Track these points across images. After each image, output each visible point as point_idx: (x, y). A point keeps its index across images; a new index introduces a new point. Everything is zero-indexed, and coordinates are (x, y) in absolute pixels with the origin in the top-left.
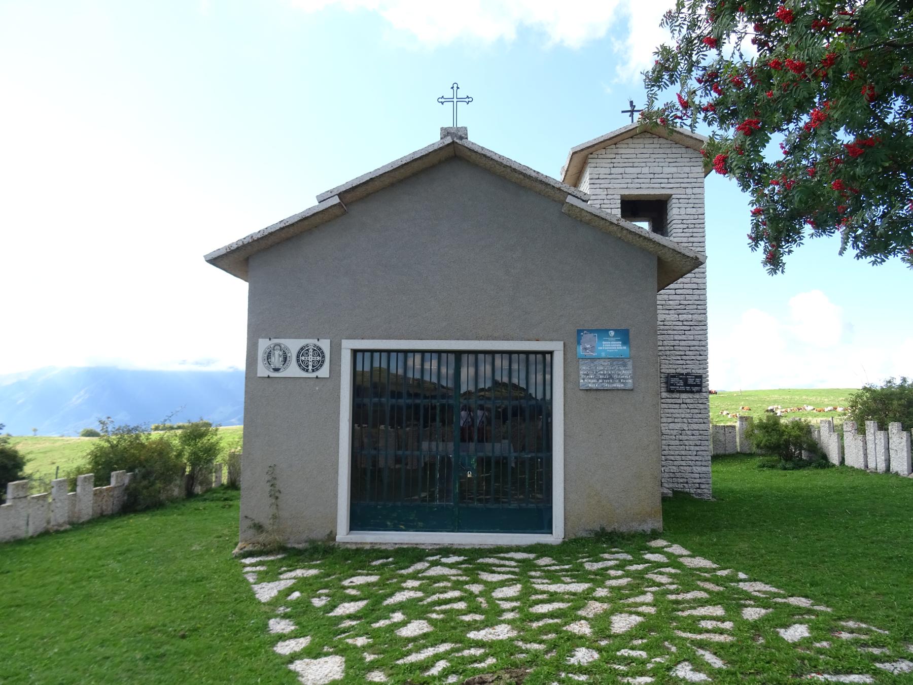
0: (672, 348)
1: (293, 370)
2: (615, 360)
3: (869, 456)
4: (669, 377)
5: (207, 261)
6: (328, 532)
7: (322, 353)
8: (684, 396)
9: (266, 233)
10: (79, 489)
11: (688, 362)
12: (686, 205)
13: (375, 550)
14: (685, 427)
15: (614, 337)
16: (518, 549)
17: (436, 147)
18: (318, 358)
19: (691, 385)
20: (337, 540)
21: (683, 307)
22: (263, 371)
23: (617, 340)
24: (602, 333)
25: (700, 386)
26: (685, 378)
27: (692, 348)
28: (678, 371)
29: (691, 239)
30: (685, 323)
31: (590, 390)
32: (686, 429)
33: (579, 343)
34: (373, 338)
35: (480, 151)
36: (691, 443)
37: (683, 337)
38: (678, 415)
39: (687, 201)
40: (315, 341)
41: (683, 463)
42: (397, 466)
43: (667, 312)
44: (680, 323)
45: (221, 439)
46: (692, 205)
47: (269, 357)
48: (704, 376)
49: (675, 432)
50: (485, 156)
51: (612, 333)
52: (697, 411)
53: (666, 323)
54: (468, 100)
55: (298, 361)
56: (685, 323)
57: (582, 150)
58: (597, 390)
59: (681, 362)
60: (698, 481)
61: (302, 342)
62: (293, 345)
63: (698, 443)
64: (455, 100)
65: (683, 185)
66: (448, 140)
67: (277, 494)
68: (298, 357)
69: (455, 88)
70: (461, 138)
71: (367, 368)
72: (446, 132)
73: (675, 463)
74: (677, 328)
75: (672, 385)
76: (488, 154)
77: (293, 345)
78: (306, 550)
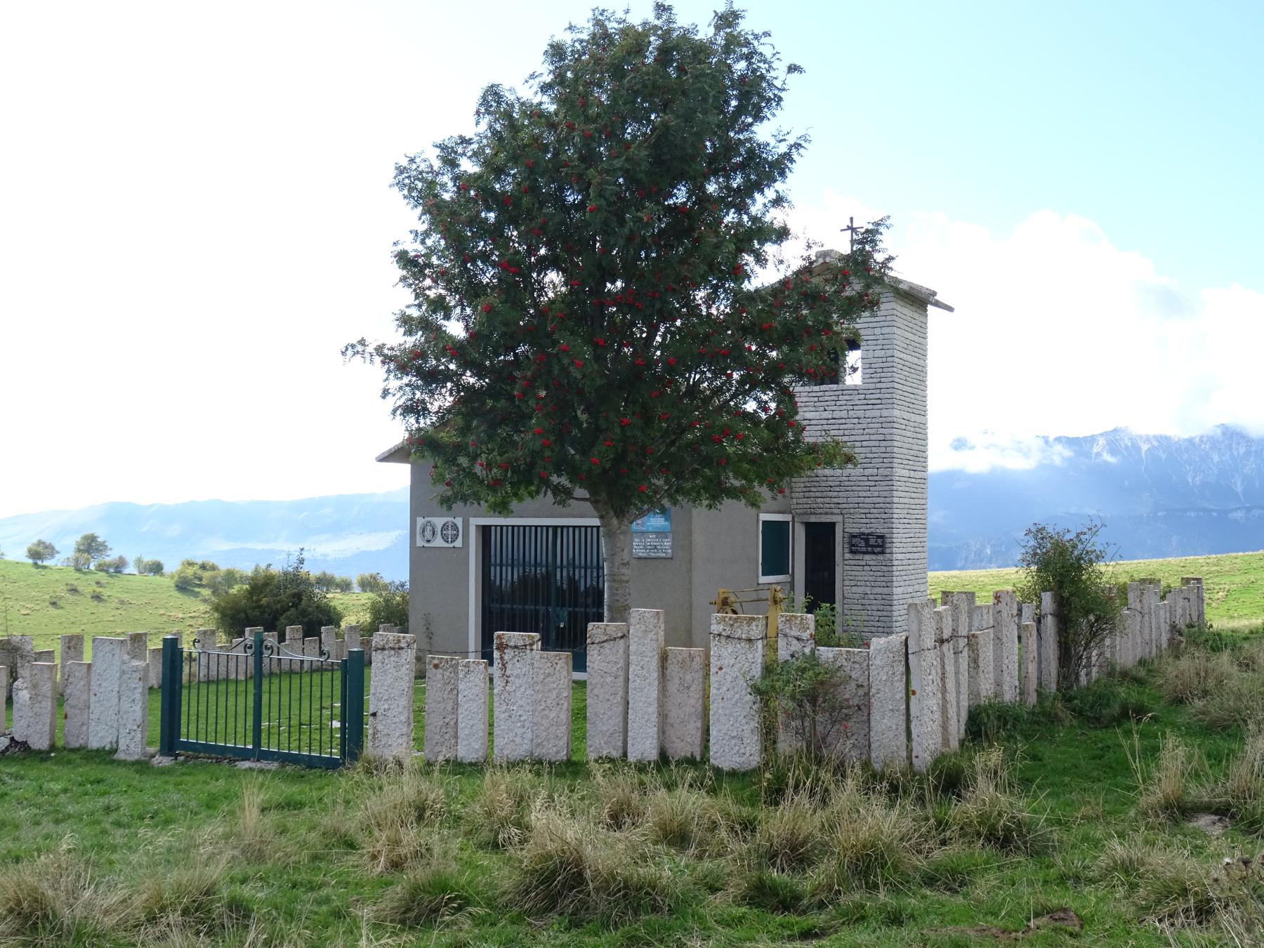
1: (439, 542)
2: (661, 534)
4: (853, 536)
8: (867, 557)
12: (875, 348)
14: (868, 590)
18: (455, 532)
19: (872, 546)
21: (868, 460)
22: (420, 542)
26: (865, 537)
27: (877, 506)
28: (862, 530)
29: (879, 385)
30: (870, 478)
31: (640, 558)
32: (869, 592)
36: (873, 607)
37: (868, 494)
38: (861, 578)
39: (875, 342)
40: (452, 519)
41: (866, 629)
44: (866, 479)
46: (881, 347)
47: (423, 531)
52: (880, 574)
53: (851, 478)
56: (870, 478)
58: (645, 558)
59: (865, 521)
63: (881, 608)
65: (871, 325)
68: (442, 531)
74: (862, 483)
75: (853, 545)
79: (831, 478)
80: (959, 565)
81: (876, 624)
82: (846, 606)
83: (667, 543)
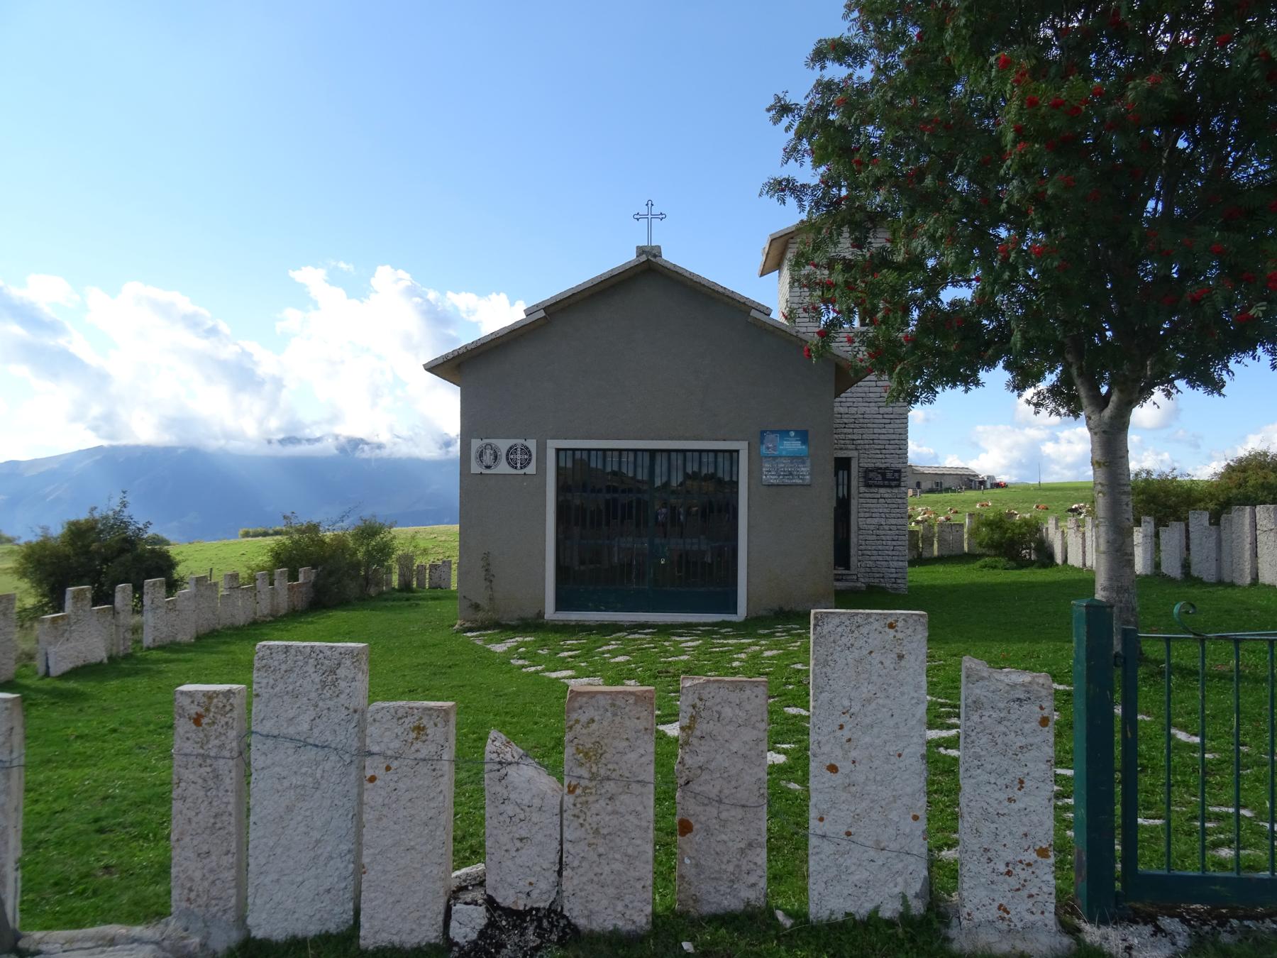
0: (871, 442)
1: (503, 468)
2: (796, 458)
3: (1087, 554)
5: (426, 370)
6: (537, 611)
7: (530, 451)
8: (882, 490)
9: (479, 344)
10: (276, 583)
11: (887, 456)
13: (579, 626)
15: (794, 437)
16: (705, 625)
17: (632, 265)
18: (526, 457)
20: (545, 617)
22: (475, 468)
23: (797, 440)
24: (784, 433)
25: (899, 480)
26: (882, 472)
27: (892, 442)
30: (886, 416)
31: (772, 485)
33: (762, 443)
34: (575, 438)
35: (672, 268)
36: (888, 537)
37: (883, 431)
38: (876, 510)
40: (522, 441)
41: (880, 558)
42: (582, 568)
43: (867, 404)
44: (881, 416)
45: (394, 537)
47: (481, 456)
48: (903, 470)
49: (872, 527)
50: (677, 272)
51: (792, 434)
52: (895, 506)
53: (866, 416)
54: (662, 216)
55: (507, 459)
56: (886, 416)
57: (781, 237)
58: (778, 485)
59: (880, 456)
60: (894, 575)
61: (511, 442)
62: (503, 445)
63: (896, 538)
64: (650, 216)
66: (644, 258)
67: (492, 578)
68: (507, 455)
69: (650, 205)
70: (655, 256)
71: (570, 465)
72: (641, 251)
73: (872, 558)
74: (877, 421)
75: (870, 479)
76: (680, 271)
77: (503, 445)
78: (518, 626)
79: (846, 416)
80: (446, 521)
81: (890, 553)
82: (861, 537)
83: (805, 470)
